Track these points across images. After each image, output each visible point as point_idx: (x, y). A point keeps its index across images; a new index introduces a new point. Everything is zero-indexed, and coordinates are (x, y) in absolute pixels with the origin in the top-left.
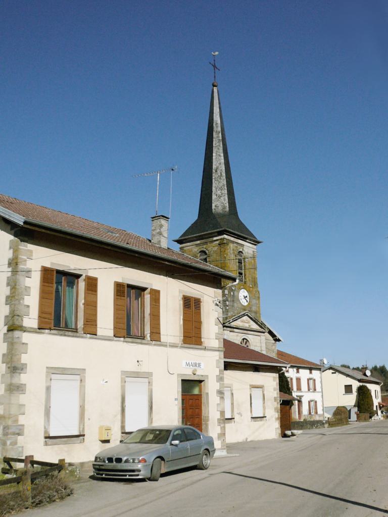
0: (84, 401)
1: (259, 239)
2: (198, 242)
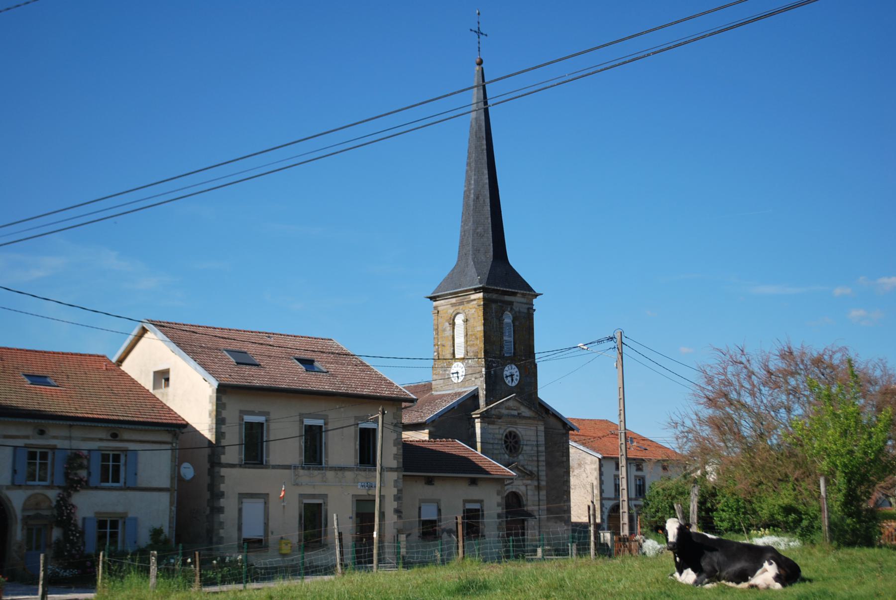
0: (268, 520)
1: (537, 291)
2: (454, 300)
